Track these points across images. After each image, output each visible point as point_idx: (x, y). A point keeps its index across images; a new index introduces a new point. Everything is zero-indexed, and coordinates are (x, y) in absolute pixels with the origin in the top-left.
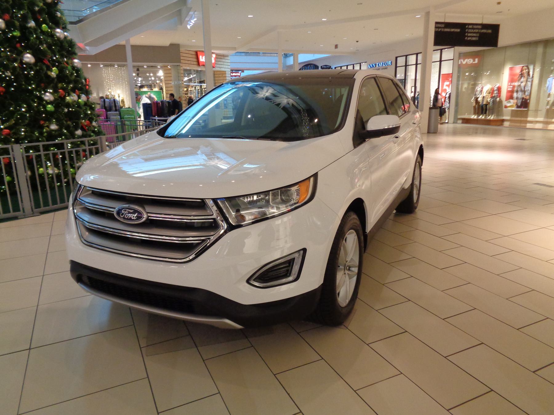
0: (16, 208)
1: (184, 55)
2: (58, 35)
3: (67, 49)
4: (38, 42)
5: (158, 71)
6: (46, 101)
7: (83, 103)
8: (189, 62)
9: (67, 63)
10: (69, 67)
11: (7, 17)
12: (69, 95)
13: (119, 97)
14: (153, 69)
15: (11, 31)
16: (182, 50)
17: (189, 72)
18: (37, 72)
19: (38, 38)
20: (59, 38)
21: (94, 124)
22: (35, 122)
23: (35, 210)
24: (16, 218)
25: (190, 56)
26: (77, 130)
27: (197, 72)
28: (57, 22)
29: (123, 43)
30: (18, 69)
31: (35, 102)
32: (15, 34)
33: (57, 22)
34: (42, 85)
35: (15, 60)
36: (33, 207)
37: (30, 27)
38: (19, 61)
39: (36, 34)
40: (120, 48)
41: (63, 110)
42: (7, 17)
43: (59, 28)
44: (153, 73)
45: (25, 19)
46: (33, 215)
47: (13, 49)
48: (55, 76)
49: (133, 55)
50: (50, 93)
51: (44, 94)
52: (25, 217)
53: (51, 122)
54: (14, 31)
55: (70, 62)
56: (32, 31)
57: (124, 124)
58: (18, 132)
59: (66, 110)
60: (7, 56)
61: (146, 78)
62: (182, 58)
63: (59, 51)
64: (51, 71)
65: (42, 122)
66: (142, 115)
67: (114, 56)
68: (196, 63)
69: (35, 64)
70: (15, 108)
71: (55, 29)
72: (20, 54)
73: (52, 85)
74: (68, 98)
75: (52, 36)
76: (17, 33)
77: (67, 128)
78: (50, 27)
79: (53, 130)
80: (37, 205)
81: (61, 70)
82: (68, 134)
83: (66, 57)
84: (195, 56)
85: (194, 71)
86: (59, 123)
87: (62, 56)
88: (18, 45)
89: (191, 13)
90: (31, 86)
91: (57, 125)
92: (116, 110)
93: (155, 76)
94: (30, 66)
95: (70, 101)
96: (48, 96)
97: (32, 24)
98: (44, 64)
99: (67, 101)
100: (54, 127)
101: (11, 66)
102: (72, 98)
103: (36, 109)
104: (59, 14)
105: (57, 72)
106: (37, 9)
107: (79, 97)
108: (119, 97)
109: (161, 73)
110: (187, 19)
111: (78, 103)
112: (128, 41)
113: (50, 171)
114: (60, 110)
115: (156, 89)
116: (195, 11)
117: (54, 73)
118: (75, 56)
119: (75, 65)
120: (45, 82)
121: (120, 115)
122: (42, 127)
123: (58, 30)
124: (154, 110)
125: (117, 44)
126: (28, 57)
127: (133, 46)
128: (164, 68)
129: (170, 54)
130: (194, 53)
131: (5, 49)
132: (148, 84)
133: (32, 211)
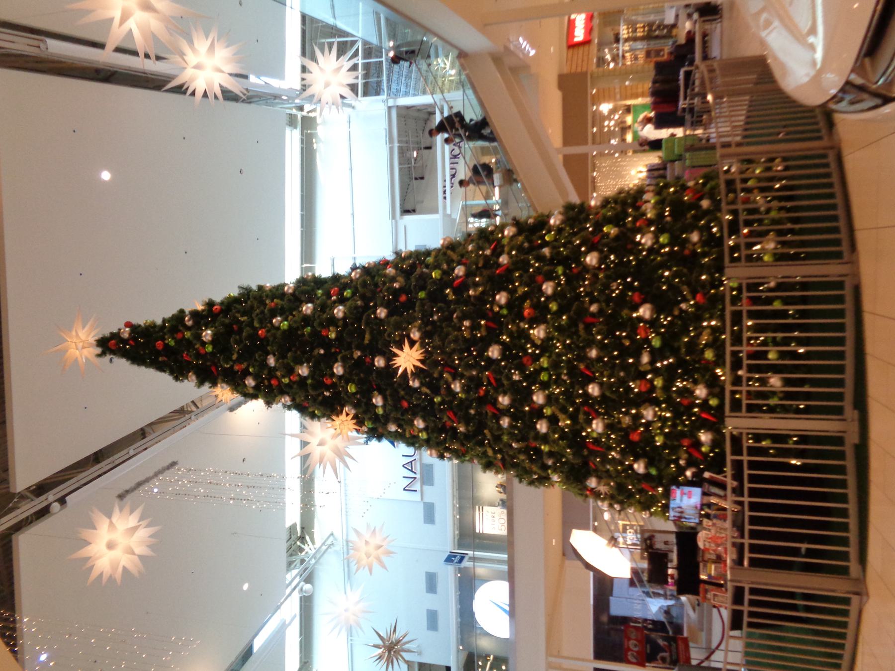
0: (840, 285)
1: (574, 66)
2: (558, 222)
3: (576, 214)
4: (570, 246)
5: (601, 113)
6: (654, 244)
7: (657, 198)
8: (585, 58)
9: (597, 214)
10: (603, 211)
11: (539, 278)
12: (644, 214)
13: (641, 172)
14: (599, 119)
15: (558, 277)
16: (566, 71)
17: (601, 61)
18: (611, 251)
19: (564, 245)
20: (563, 222)
21: (691, 184)
22: (687, 261)
23: (846, 259)
24: (857, 291)
25: (575, 58)
26: (701, 207)
27: (601, 46)
28: (542, 223)
29: (560, 157)
30: (609, 273)
31: (655, 259)
32: (560, 272)
33: (542, 223)
34: (629, 247)
35: (595, 276)
36: (839, 261)
37: (551, 253)
38: (597, 272)
39: (560, 247)
40: (569, 162)
41: (667, 222)
42: (539, 278)
43: (549, 222)
44: (604, 122)
45: (540, 258)
46: (854, 263)
47: (580, 277)
48: (616, 229)
49: (578, 144)
50: (641, 238)
51: (643, 245)
52: (856, 275)
53: (687, 240)
54: (556, 272)
55: (594, 211)
56: (555, 251)
57: (692, 146)
58: (703, 284)
59: (668, 219)
60: (590, 284)
61: (611, 134)
62: (579, 70)
63: (580, 223)
64: (608, 234)
65: (687, 252)
66: (671, 131)
67: (579, 169)
68: (586, 47)
69: (601, 252)
70: (664, 283)
71: (550, 226)
72: (586, 268)
73: (629, 234)
74: (649, 216)
75: (560, 230)
76: (560, 270)
77: (697, 218)
78: (549, 232)
79: (700, 239)
80: (838, 255)
81: (608, 221)
82: (706, 218)
83: (589, 215)
84: (576, 50)
85: (599, 50)
86: (690, 229)
87: (587, 220)
88: (575, 271)
89: (512, 47)
90: (631, 261)
91: (692, 232)
92: (665, 169)
93: (609, 118)
94: (603, 259)
95: (654, 212)
96: (645, 240)
97: (546, 251)
98: (598, 242)
99: (653, 217)
100: (695, 237)
101: (604, 280)
102: (648, 210)
103: (665, 258)
104: (531, 221)
105: (611, 226)
106: (526, 245)
107: (647, 201)
108: (641, 172)
109: (605, 108)
110: (521, 56)
111: (657, 203)
112: (558, 151)
113: (771, 246)
114: (668, 226)
115: (629, 119)
116: (508, 39)
117: (611, 230)
118: (586, 205)
119: (598, 204)
120: (624, 243)
121: (673, 161)
122: (694, 253)
123: (552, 221)
124: (667, 108)
125: (561, 164)
126: (591, 260)
127: (566, 142)
128: (597, 100)
129: (576, 91)
130: (571, 51)
131: (581, 287)
132: (619, 133)
133: (847, 263)
